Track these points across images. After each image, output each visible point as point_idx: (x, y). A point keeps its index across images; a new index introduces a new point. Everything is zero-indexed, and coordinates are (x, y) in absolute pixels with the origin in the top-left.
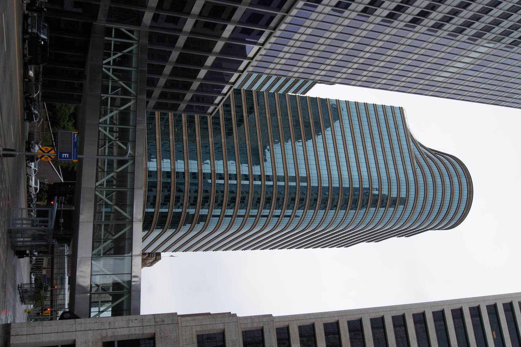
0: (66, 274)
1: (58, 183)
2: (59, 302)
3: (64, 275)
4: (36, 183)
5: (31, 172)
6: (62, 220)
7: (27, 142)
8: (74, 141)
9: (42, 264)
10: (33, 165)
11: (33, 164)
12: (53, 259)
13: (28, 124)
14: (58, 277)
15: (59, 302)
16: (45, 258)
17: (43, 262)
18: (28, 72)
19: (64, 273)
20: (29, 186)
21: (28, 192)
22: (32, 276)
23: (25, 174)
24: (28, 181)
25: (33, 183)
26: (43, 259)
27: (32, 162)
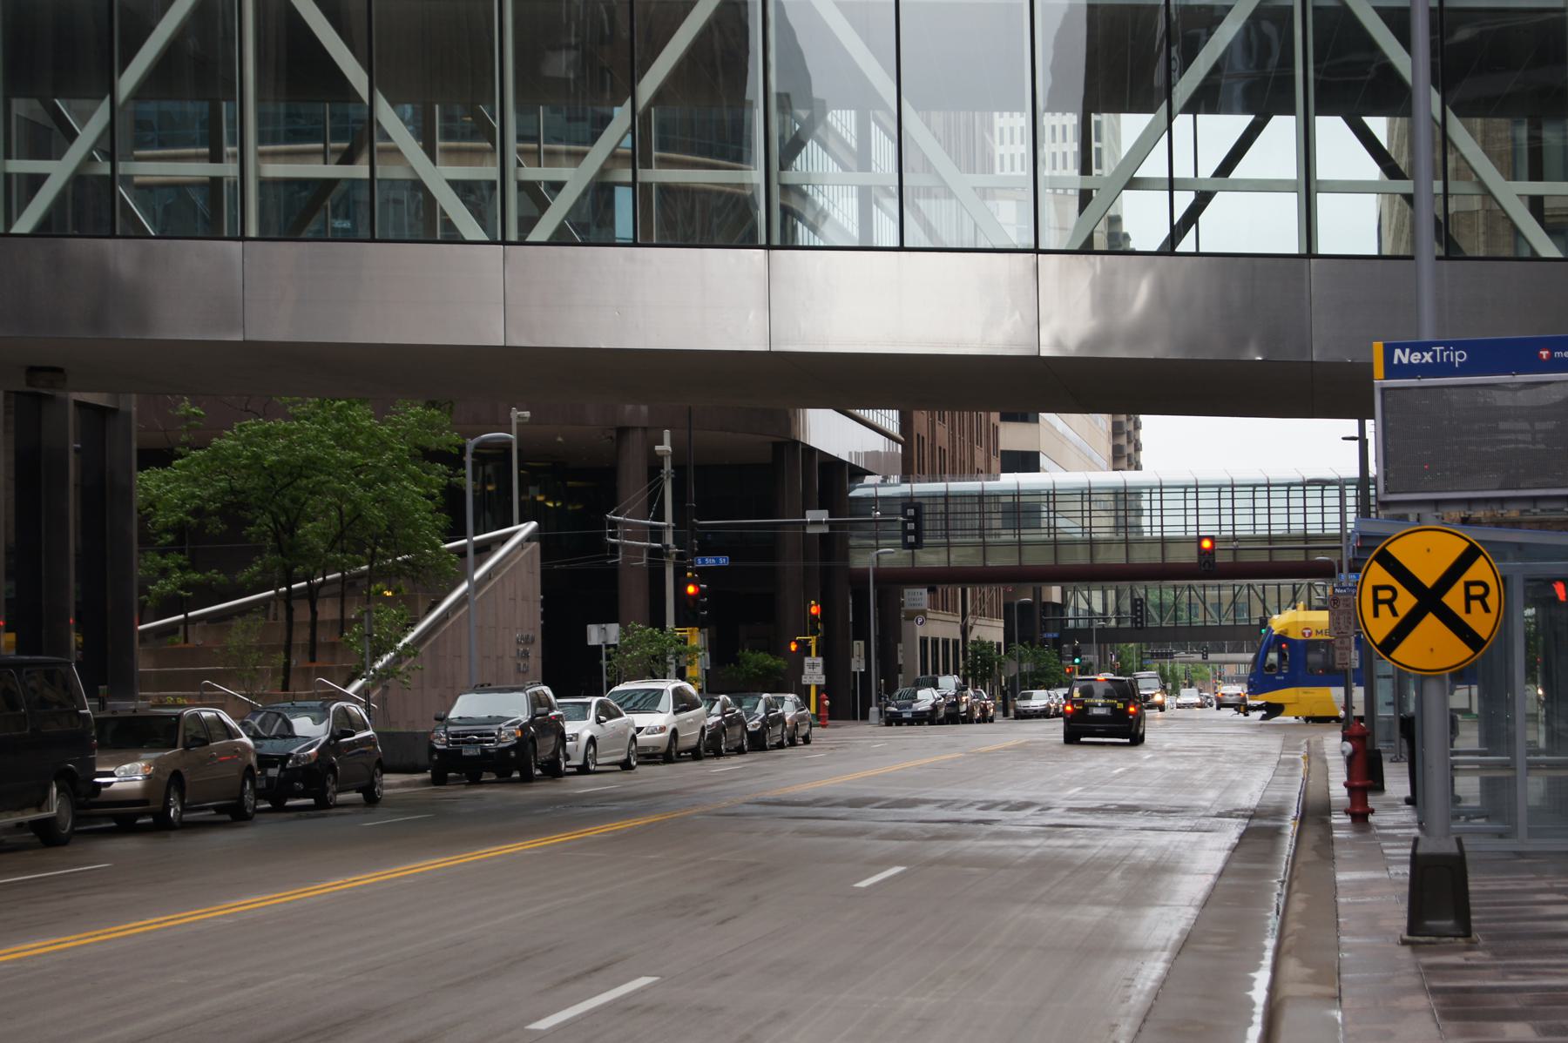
0: (991, 486)
1: (546, 555)
2: (1103, 525)
3: (996, 496)
4: (649, 702)
5: (619, 735)
6: (811, 515)
7: (439, 780)
8: (1464, 370)
9: (946, 642)
10: (580, 729)
11: (570, 728)
12: (932, 579)
13: (1412, 708)
14: (1008, 536)
15: (1103, 525)
16: (920, 631)
17: (935, 641)
18: (123, 801)
19: (981, 497)
20: (670, 753)
21: (711, 746)
22: (926, 698)
23: (624, 776)
24: (650, 757)
25: (656, 723)
26: (924, 641)
27: (562, 737)
